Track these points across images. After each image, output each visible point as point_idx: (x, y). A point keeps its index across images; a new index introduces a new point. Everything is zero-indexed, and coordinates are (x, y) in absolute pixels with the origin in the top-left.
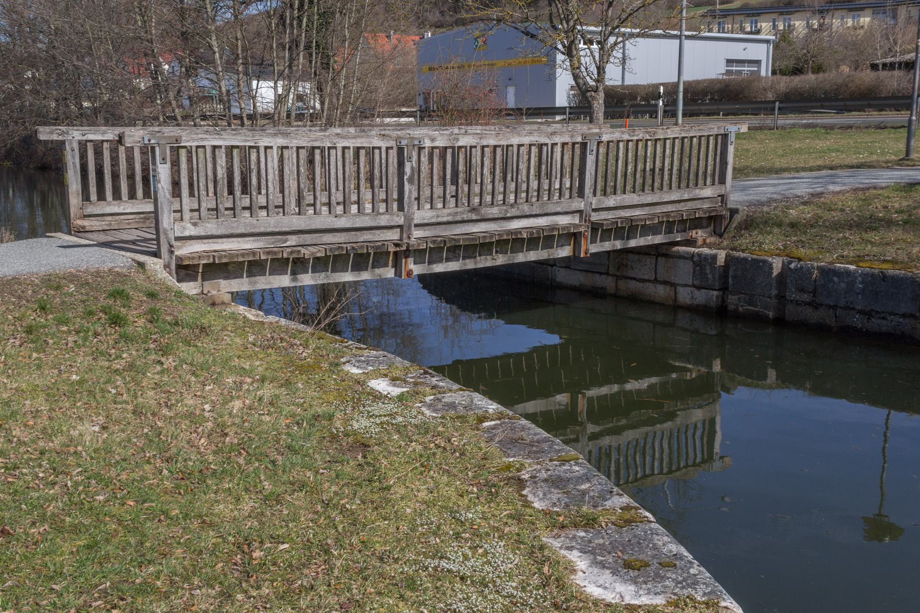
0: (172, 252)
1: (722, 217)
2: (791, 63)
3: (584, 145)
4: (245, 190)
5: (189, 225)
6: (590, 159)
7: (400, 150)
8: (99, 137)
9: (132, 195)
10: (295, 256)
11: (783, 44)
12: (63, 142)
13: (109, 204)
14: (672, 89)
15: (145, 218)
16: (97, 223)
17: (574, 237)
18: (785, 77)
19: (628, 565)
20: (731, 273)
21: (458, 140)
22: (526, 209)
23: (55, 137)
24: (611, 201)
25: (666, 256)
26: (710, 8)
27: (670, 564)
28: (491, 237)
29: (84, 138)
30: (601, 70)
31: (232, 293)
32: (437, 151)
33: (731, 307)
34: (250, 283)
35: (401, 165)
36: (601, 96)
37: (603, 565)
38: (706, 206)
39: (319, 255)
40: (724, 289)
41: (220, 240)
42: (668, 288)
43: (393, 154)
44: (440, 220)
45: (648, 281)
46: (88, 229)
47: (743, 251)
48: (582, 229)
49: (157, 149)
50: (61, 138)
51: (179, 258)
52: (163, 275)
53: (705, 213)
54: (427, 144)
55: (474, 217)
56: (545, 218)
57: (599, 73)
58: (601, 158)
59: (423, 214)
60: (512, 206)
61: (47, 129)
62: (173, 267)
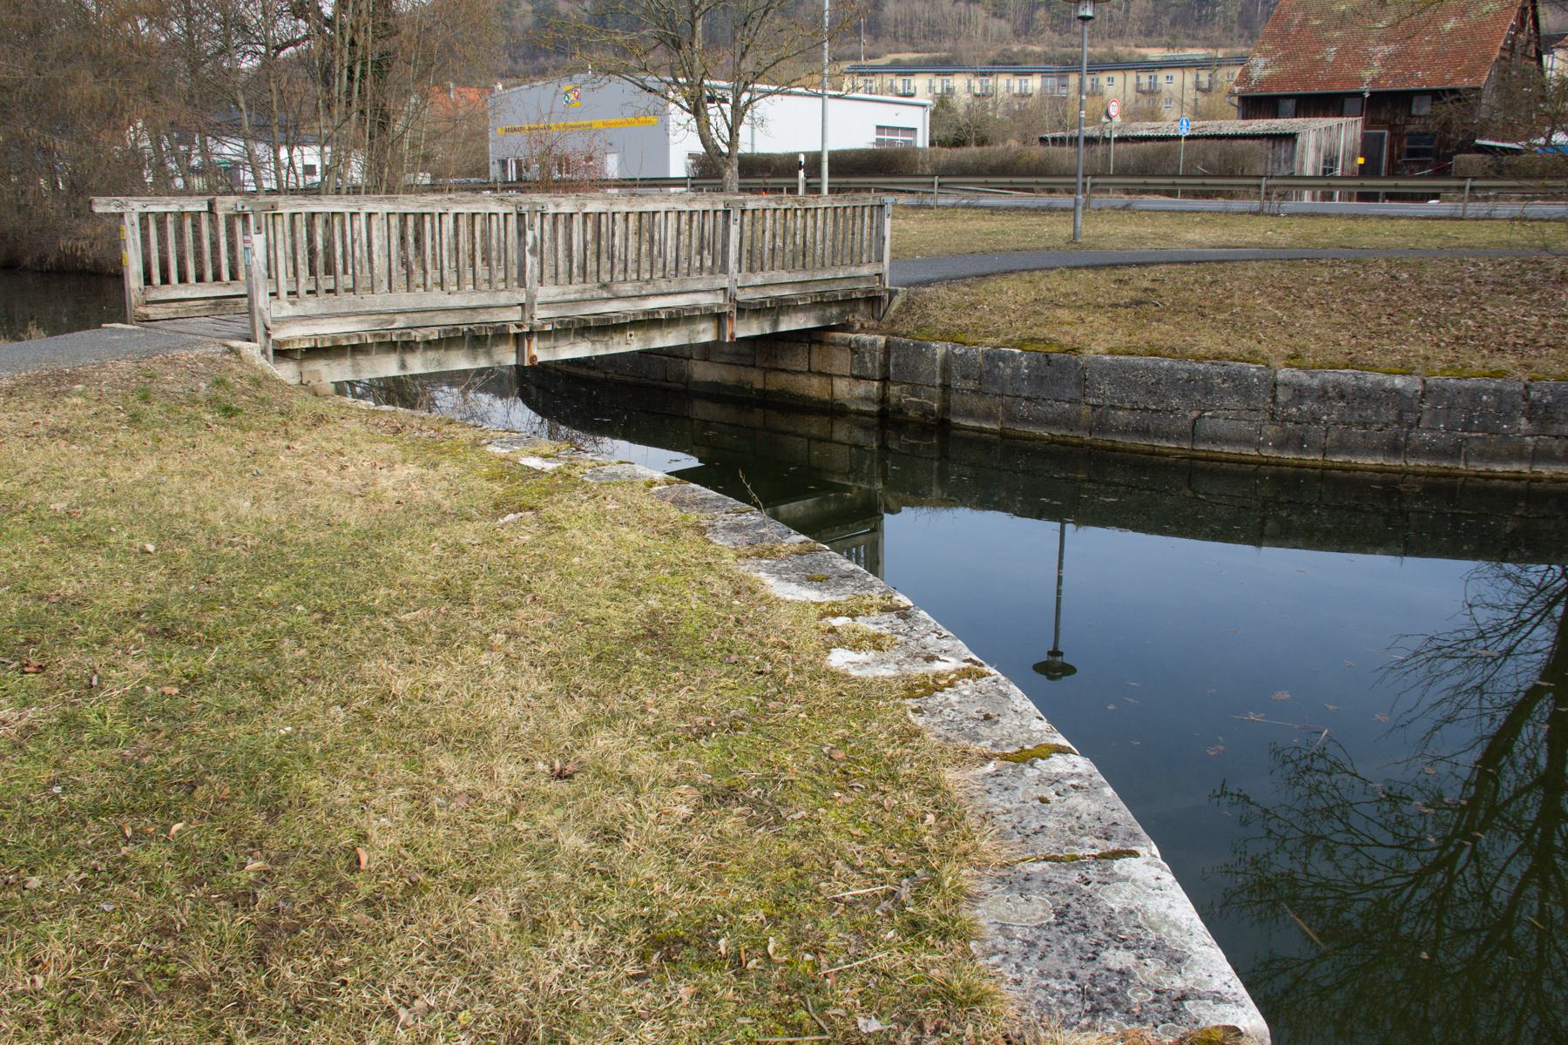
0: (268, 336)
1: (879, 299)
2: (951, 134)
3: (727, 213)
4: (330, 269)
5: (287, 304)
6: (734, 229)
7: (520, 216)
8: (162, 209)
9: (200, 278)
10: (405, 338)
11: (941, 111)
12: (122, 215)
13: (175, 288)
14: (814, 162)
15: (216, 304)
16: (162, 311)
17: (719, 318)
18: (945, 149)
19: (810, 579)
20: (892, 361)
21: (585, 205)
22: (663, 286)
23: (112, 209)
24: (758, 279)
25: (821, 343)
26: (853, 63)
27: (850, 576)
28: (625, 317)
29: (146, 210)
30: (733, 131)
31: (336, 383)
32: (561, 218)
33: (893, 400)
34: (354, 372)
35: (521, 233)
36: (736, 161)
37: (789, 580)
38: (863, 286)
39: (431, 338)
40: (885, 380)
41: (320, 322)
42: (824, 380)
43: (512, 220)
44: (567, 297)
45: (801, 372)
46: (152, 317)
47: (904, 336)
48: (727, 310)
49: (251, 218)
50: (119, 210)
51: (276, 342)
52: (260, 361)
53: (863, 293)
54: (551, 210)
55: (605, 295)
56: (685, 296)
57: (731, 135)
58: (745, 228)
59: (547, 292)
60: (647, 282)
61: (103, 200)
62: (270, 353)
